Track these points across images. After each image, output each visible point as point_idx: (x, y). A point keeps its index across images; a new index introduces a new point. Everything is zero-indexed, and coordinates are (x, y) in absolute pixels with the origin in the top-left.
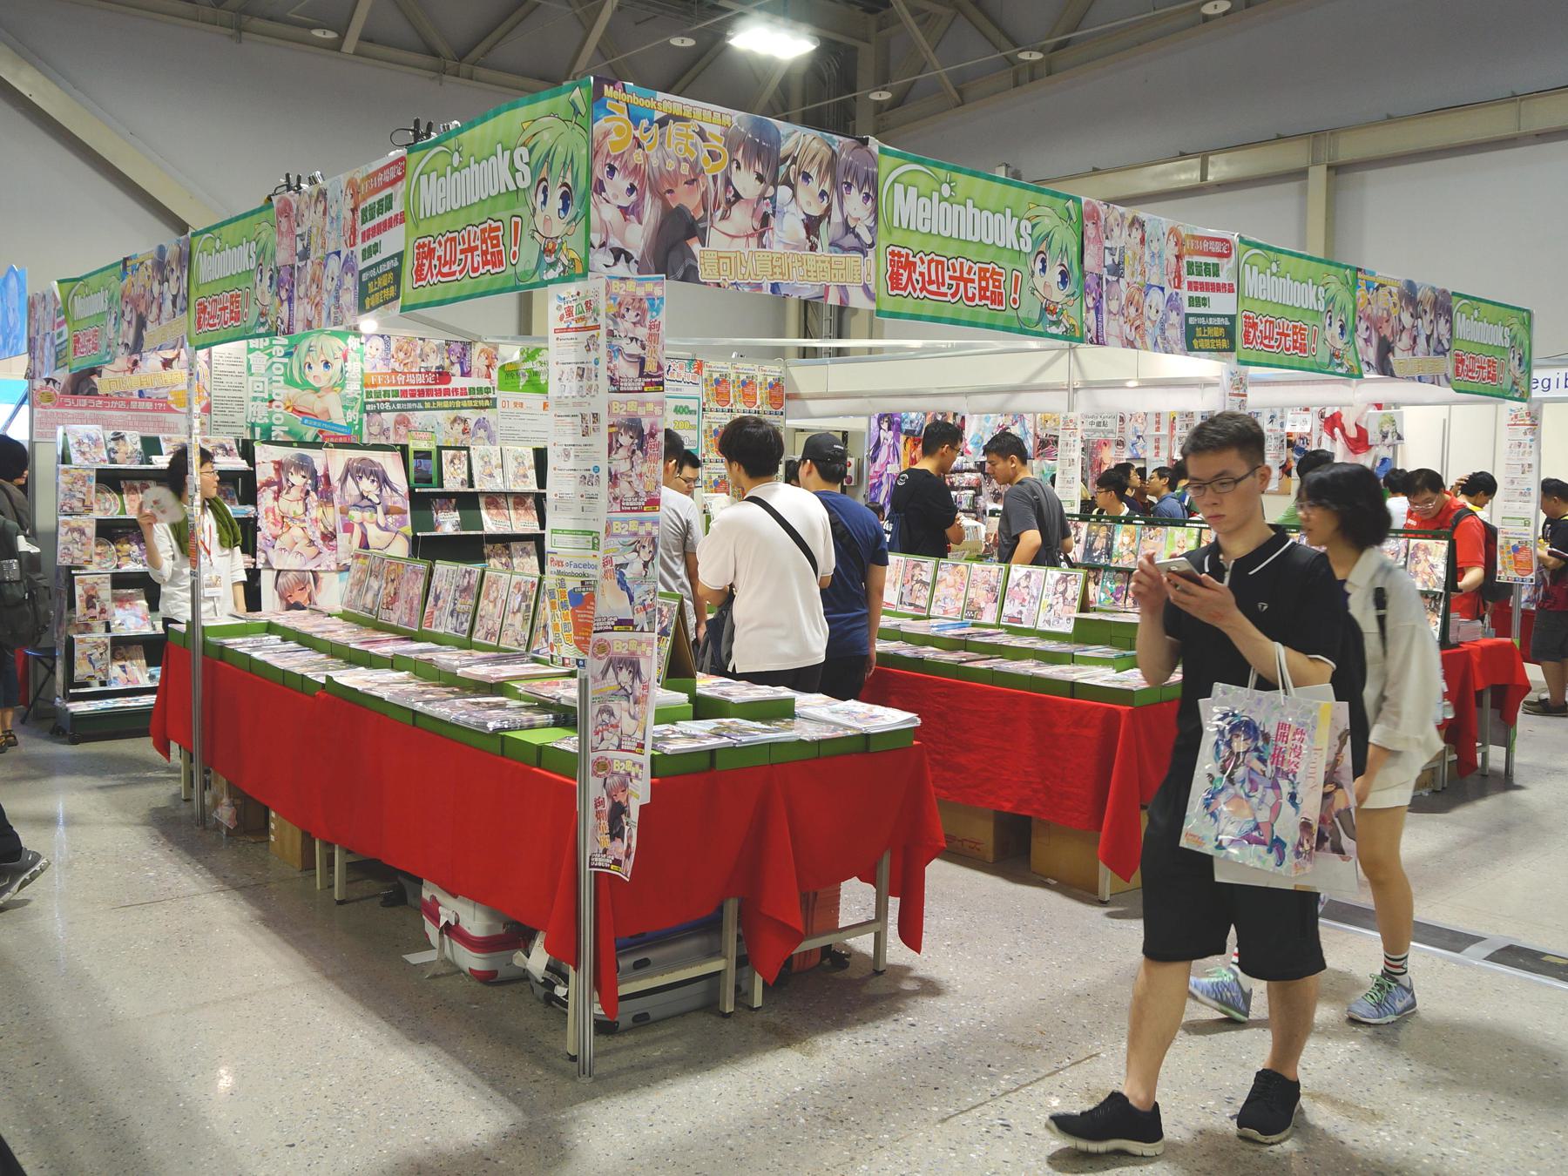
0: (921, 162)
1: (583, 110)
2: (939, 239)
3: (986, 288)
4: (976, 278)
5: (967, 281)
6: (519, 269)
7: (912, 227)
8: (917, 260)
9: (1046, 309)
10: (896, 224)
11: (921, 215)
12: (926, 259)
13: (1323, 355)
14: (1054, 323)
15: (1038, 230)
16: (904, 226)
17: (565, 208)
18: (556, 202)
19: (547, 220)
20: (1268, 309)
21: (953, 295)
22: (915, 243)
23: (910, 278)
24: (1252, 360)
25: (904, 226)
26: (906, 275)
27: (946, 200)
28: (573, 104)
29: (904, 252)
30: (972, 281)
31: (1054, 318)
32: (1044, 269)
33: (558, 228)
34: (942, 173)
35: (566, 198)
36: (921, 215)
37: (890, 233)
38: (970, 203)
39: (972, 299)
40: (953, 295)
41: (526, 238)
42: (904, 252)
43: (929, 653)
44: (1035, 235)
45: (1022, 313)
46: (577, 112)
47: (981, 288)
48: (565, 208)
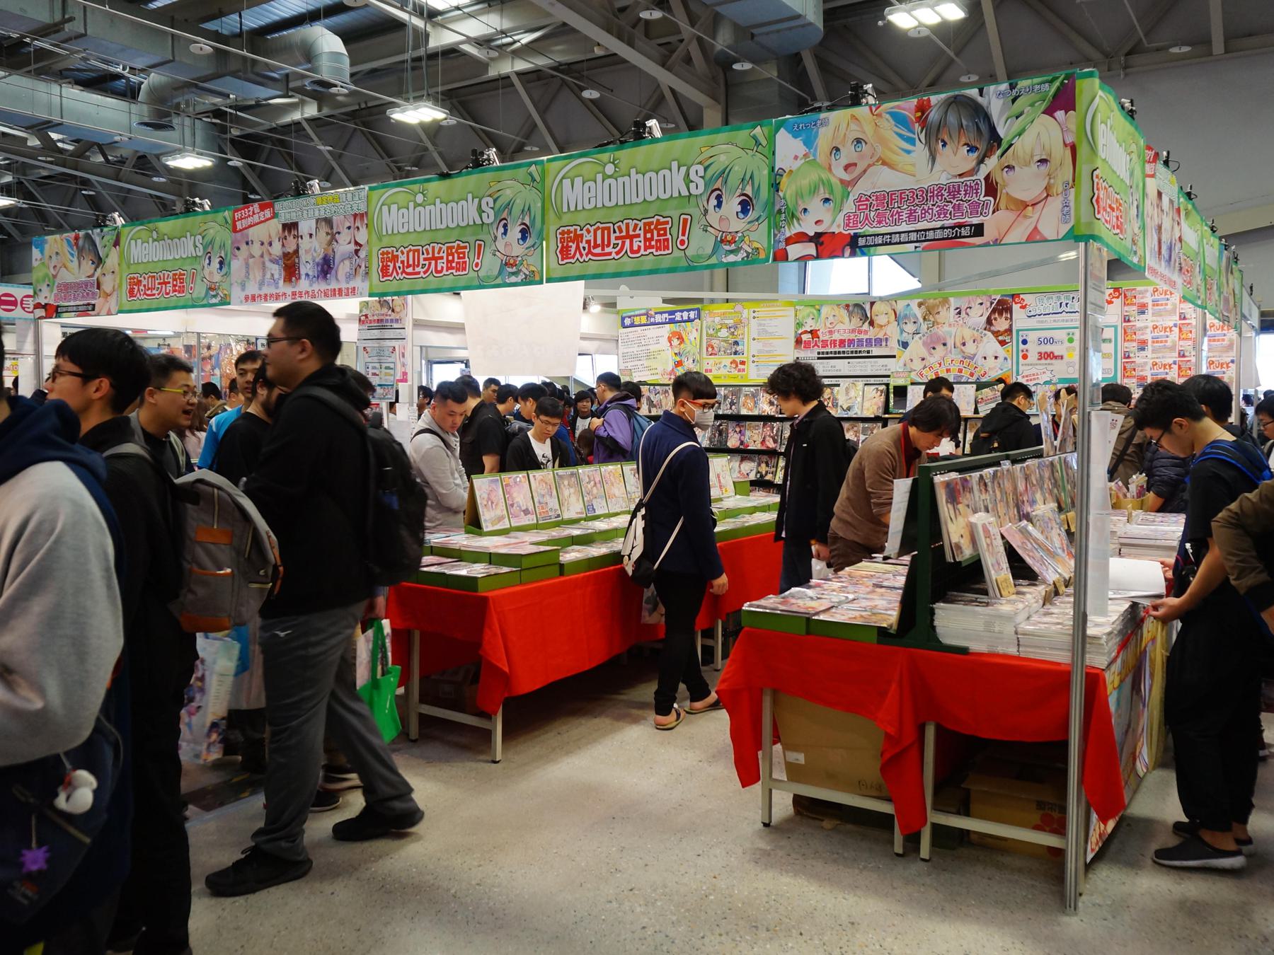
0: (581, 156)
1: (764, 142)
2: (585, 213)
3: (652, 238)
4: (642, 232)
5: (436, 259)
6: (194, 296)
7: (580, 207)
8: (584, 232)
9: (506, 264)
10: (565, 209)
11: (587, 195)
12: (592, 229)
13: (200, 290)
14: (513, 274)
15: (710, 172)
16: (572, 209)
17: (221, 268)
18: (215, 264)
19: (211, 273)
20: (151, 267)
21: (617, 253)
22: (141, 269)
23: (578, 247)
24: (418, 288)
25: (572, 209)
26: (574, 246)
27: (610, 177)
28: (530, 174)
29: (572, 229)
30: (638, 236)
31: (514, 269)
32: (505, 233)
33: (217, 278)
34: (416, 187)
35: (221, 263)
36: (587, 195)
37: (380, 240)
38: (633, 171)
39: (638, 251)
40: (617, 253)
41: (198, 281)
42: (572, 229)
43: (543, 548)
44: (708, 177)
45: (481, 274)
46: (534, 180)
47: (646, 239)
48: (221, 268)
